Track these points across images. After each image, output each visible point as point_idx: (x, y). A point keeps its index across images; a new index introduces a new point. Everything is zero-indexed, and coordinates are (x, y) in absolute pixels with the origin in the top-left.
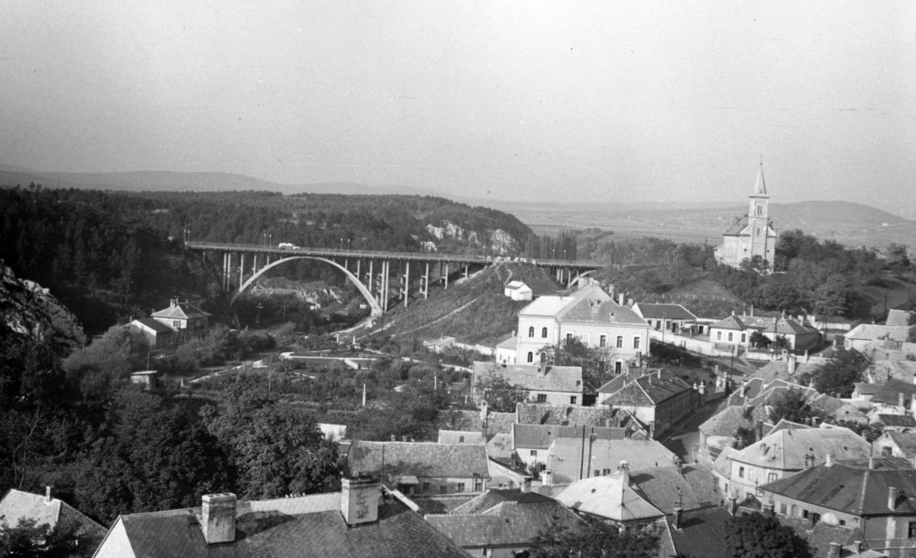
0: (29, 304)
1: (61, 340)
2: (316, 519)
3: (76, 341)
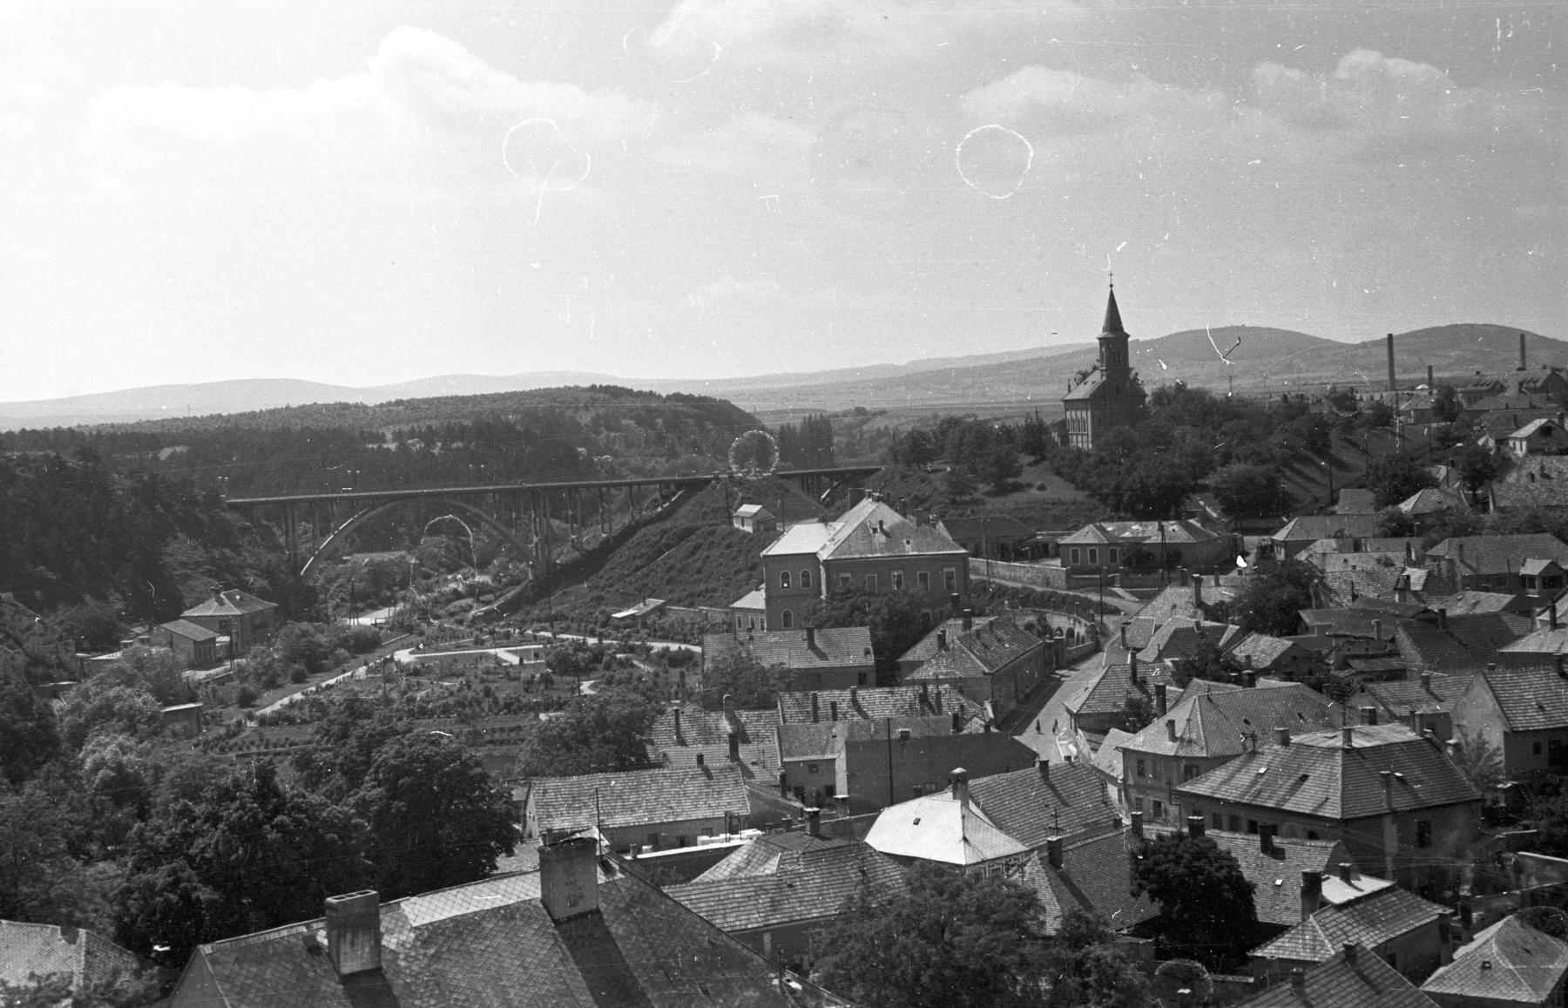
1: (40, 671)
2: (504, 917)
3: (66, 670)
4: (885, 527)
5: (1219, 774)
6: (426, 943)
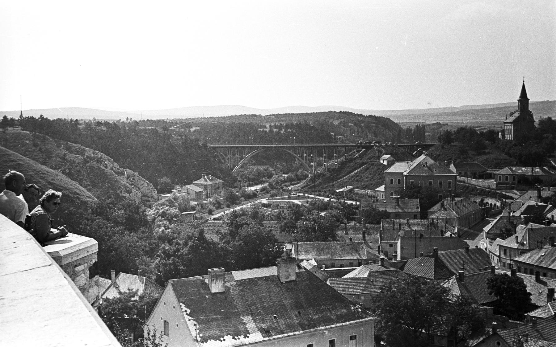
0: (128, 181)
1: (146, 198)
2: (265, 280)
3: (153, 198)
4: (427, 165)
5: (528, 255)
6: (239, 285)
